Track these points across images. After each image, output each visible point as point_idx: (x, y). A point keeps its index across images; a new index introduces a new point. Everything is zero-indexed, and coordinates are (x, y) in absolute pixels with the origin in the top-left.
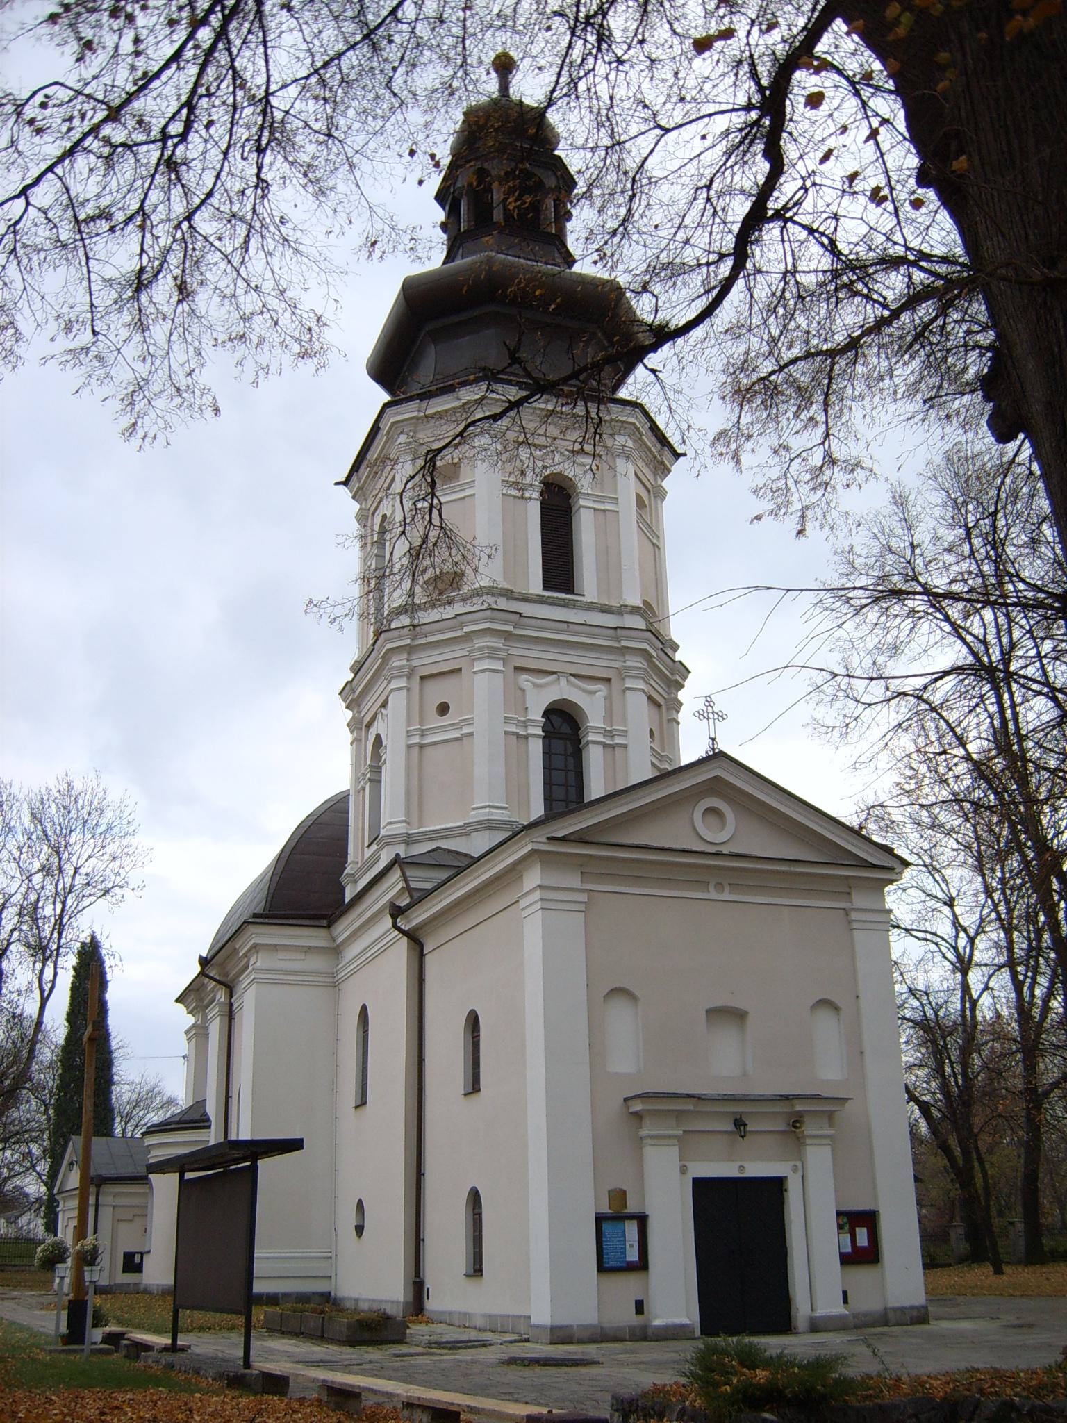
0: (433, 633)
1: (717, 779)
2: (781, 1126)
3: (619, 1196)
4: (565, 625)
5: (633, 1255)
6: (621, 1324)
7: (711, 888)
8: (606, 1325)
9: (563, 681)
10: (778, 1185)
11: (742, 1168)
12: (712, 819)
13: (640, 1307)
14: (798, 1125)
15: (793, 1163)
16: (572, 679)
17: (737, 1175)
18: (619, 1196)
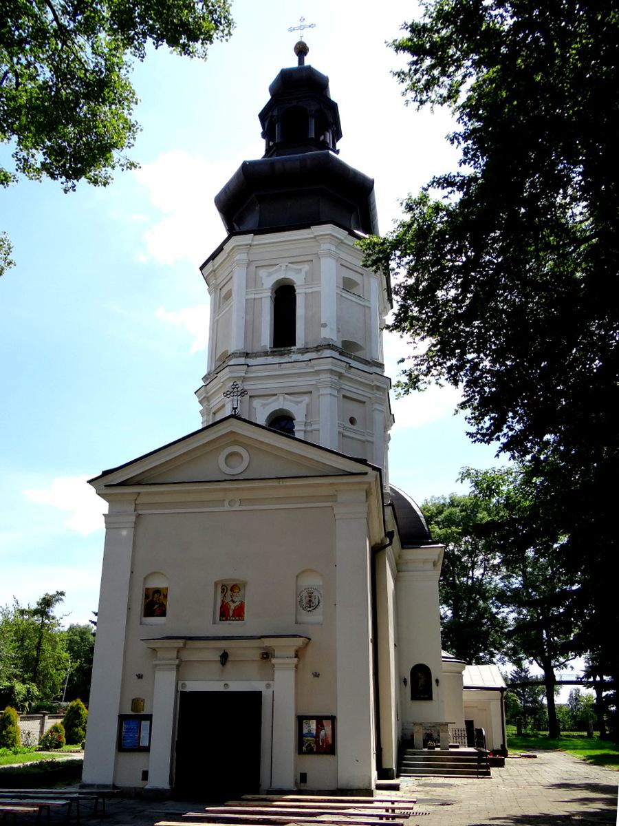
0: (257, 371)
1: (232, 432)
2: (257, 657)
4: (278, 365)
6: (131, 786)
7: (226, 503)
8: (119, 784)
9: (281, 398)
10: (257, 696)
12: (234, 460)
13: (145, 775)
14: (265, 656)
15: (267, 682)
16: (286, 396)
17: (222, 689)
18: (136, 703)
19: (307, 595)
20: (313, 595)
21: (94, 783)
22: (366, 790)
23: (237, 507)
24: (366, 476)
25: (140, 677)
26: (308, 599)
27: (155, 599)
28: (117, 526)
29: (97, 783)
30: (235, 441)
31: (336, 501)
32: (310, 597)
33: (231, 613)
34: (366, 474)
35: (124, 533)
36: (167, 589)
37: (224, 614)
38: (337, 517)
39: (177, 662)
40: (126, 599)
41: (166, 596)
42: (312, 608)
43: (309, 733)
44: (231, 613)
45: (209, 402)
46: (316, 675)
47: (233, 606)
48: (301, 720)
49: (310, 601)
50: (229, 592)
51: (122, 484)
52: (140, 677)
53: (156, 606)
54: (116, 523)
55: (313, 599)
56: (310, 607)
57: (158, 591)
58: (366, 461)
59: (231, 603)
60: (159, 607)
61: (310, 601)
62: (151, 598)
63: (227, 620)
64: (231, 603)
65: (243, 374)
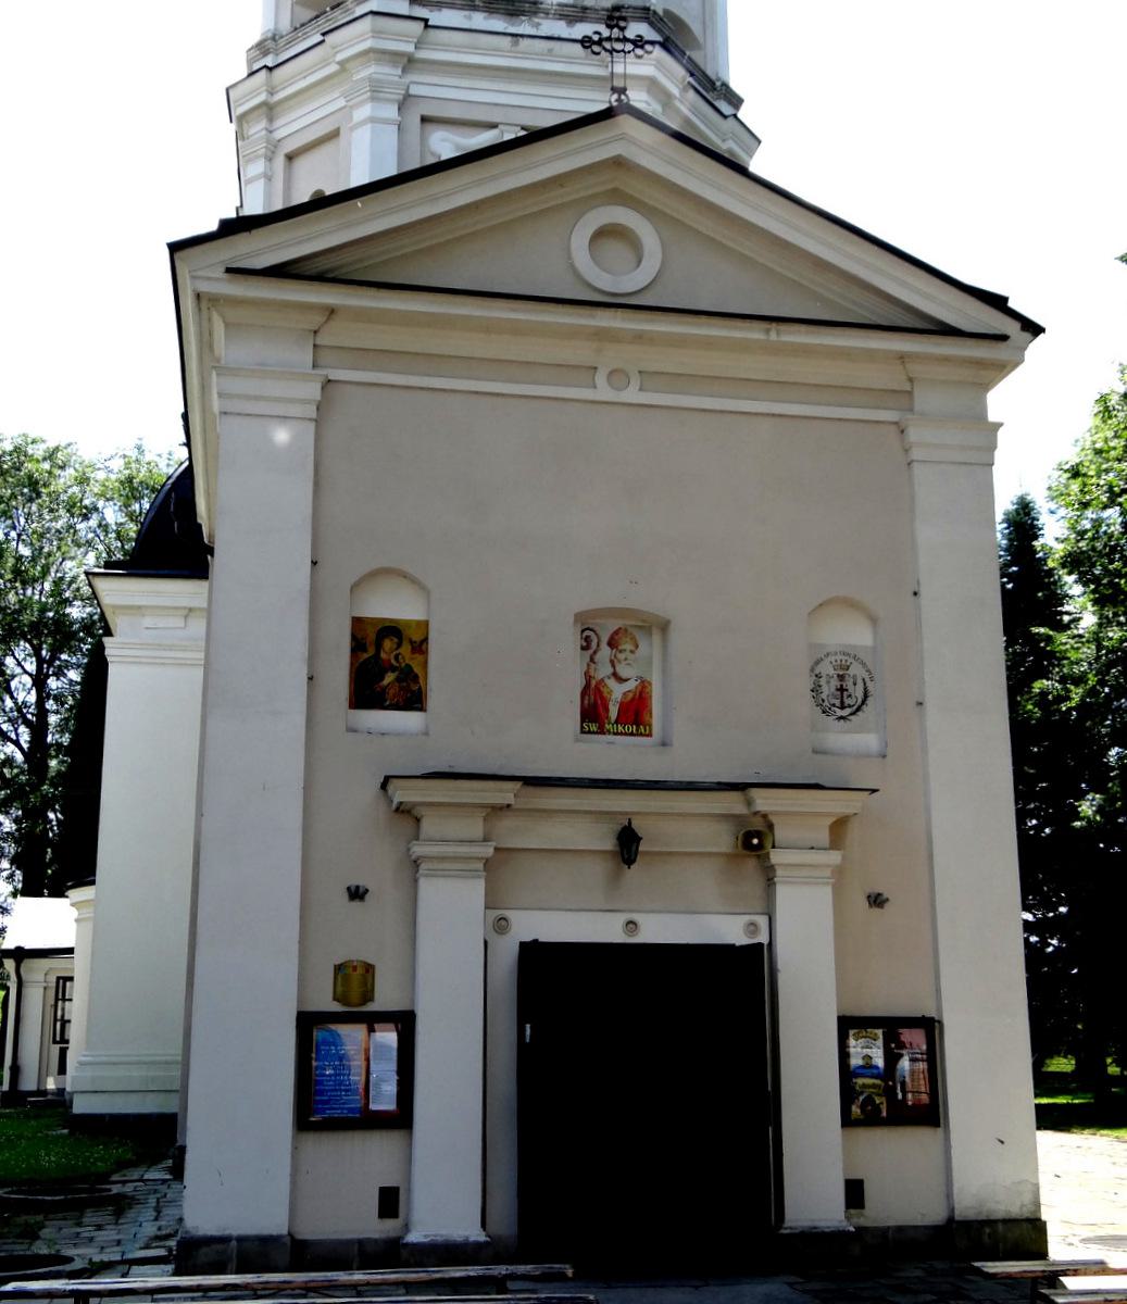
0: (446, 47)
1: (618, 163)
3: (355, 980)
4: (509, 38)
5: (385, 1099)
7: (601, 379)
11: (631, 925)
12: (615, 250)
13: (389, 1202)
15: (747, 918)
18: (355, 980)
19: (832, 672)
20: (851, 671)
21: (227, 1232)
22: (1028, 1220)
23: (632, 395)
24: (1002, 345)
25: (357, 894)
26: (835, 683)
27: (383, 655)
28: (250, 407)
29: (235, 1233)
30: (615, 191)
31: (911, 410)
32: (841, 678)
33: (613, 712)
34: (1003, 338)
35: (282, 435)
36: (425, 625)
37: (593, 714)
38: (916, 454)
39: (488, 851)
40: (300, 648)
41: (421, 647)
42: (847, 712)
43: (868, 1065)
44: (613, 712)
45: (271, 120)
46: (877, 901)
47: (617, 692)
48: (848, 1025)
49: (842, 690)
50: (605, 652)
51: (281, 272)
52: (357, 894)
53: (389, 678)
54: (257, 398)
55: (849, 684)
56: (842, 707)
57: (391, 630)
58: (1006, 299)
59: (612, 683)
60: (398, 679)
61: (842, 690)
62: (371, 652)
63: (601, 731)
64: (612, 683)
65: (410, 48)
